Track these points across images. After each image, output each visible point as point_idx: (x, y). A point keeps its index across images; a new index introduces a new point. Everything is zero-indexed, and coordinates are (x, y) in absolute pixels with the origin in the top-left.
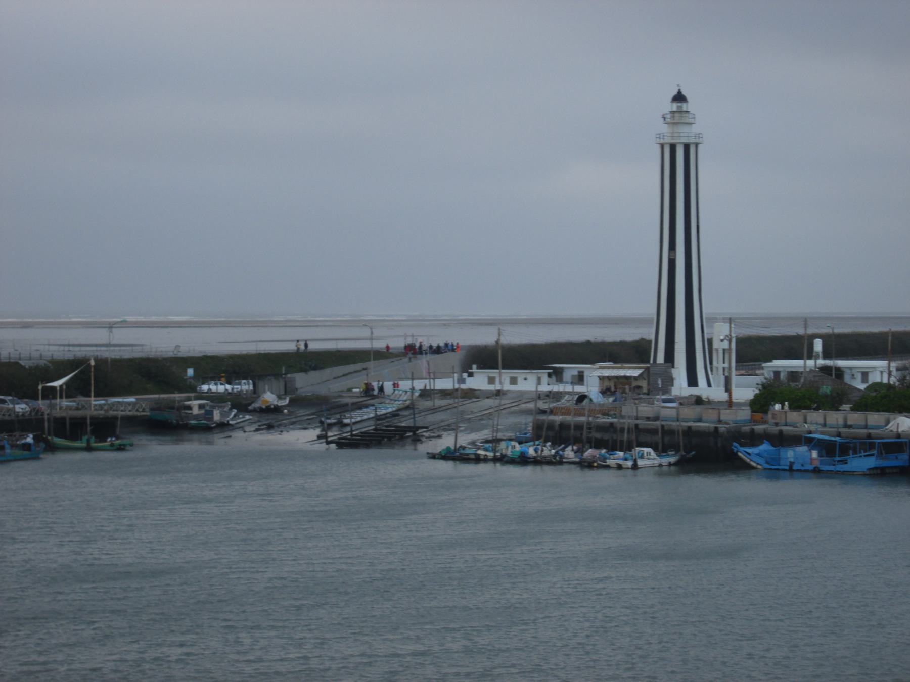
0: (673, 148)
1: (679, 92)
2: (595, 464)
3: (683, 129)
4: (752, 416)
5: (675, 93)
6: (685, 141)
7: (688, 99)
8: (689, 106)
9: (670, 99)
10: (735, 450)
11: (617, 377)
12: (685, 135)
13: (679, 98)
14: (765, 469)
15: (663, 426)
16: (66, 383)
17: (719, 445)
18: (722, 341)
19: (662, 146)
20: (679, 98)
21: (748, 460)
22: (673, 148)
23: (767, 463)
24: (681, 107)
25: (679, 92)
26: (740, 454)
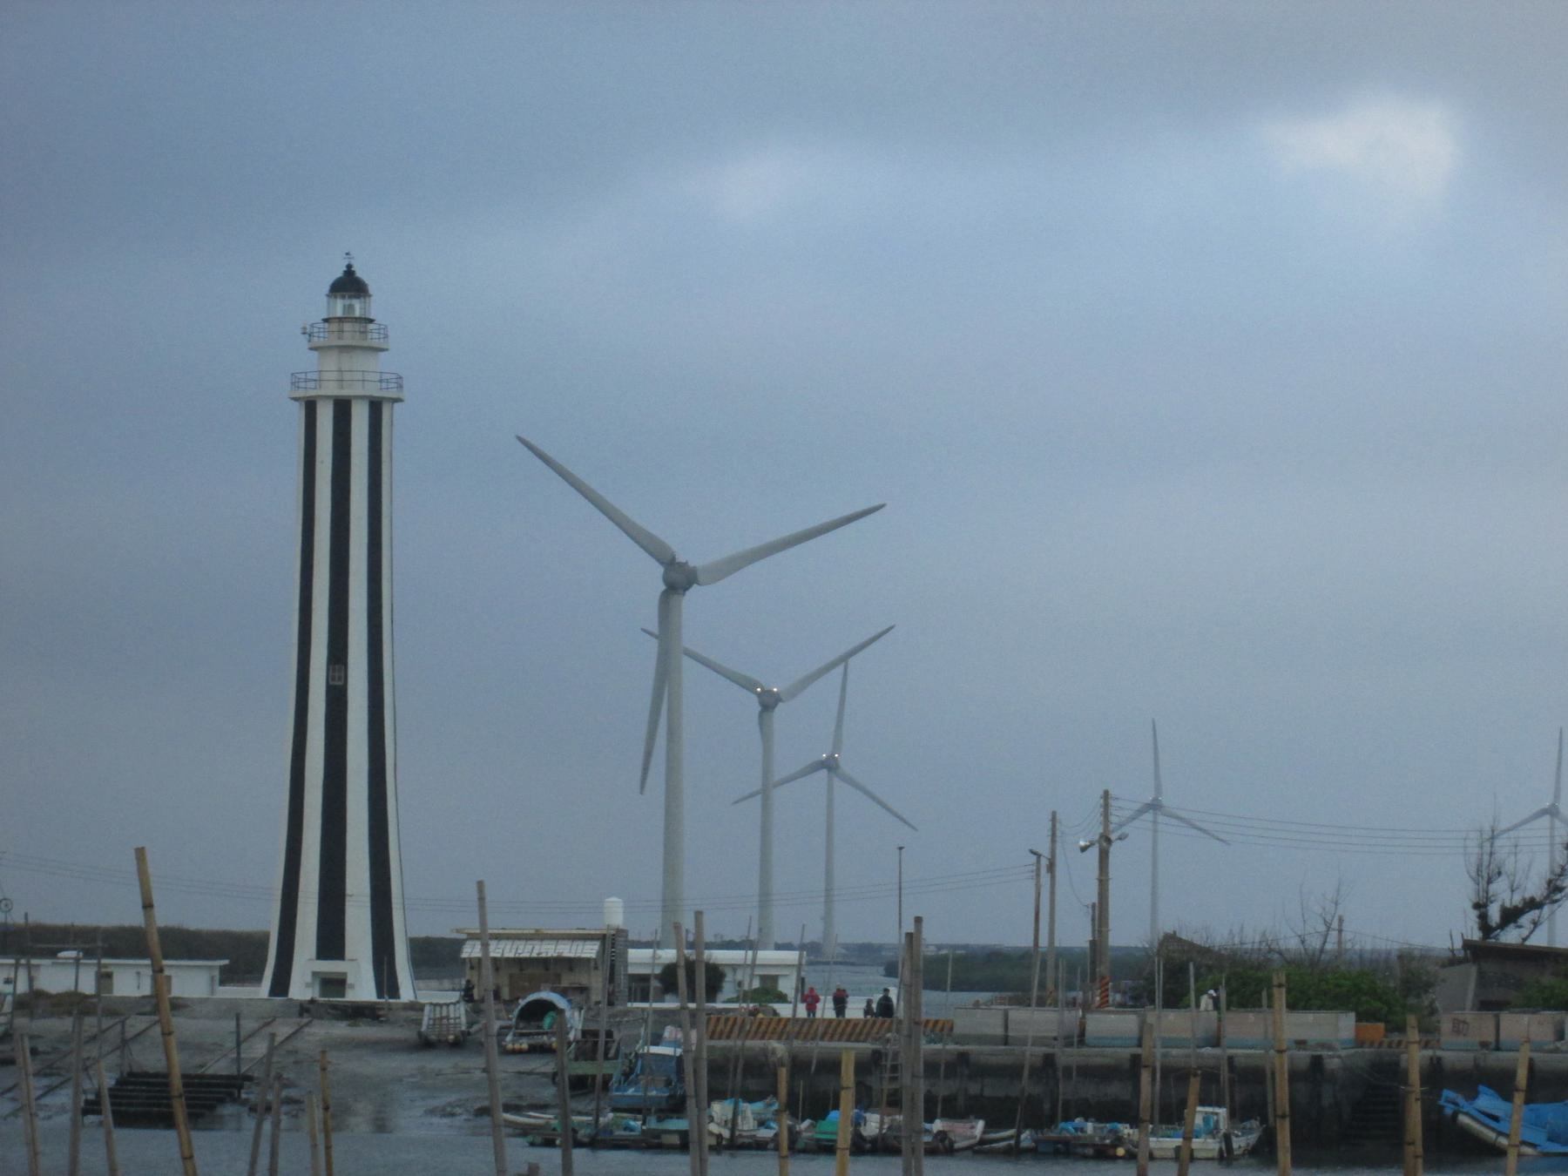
0: (342, 409)
1: (349, 272)
2: (1121, 1151)
3: (361, 362)
4: (1358, 1030)
5: (339, 272)
6: (374, 391)
7: (372, 289)
8: (377, 306)
9: (326, 289)
10: (1449, 1110)
11: (520, 962)
12: (361, 378)
13: (349, 285)
14: (1547, 1155)
15: (1231, 1059)
16: (538, 990)
17: (1327, 1101)
18: (1084, 849)
19: (310, 407)
20: (349, 285)
21: (1492, 1135)
22: (342, 409)
23: (1552, 1138)
24: (351, 307)
25: (349, 272)
26: (1463, 1119)
